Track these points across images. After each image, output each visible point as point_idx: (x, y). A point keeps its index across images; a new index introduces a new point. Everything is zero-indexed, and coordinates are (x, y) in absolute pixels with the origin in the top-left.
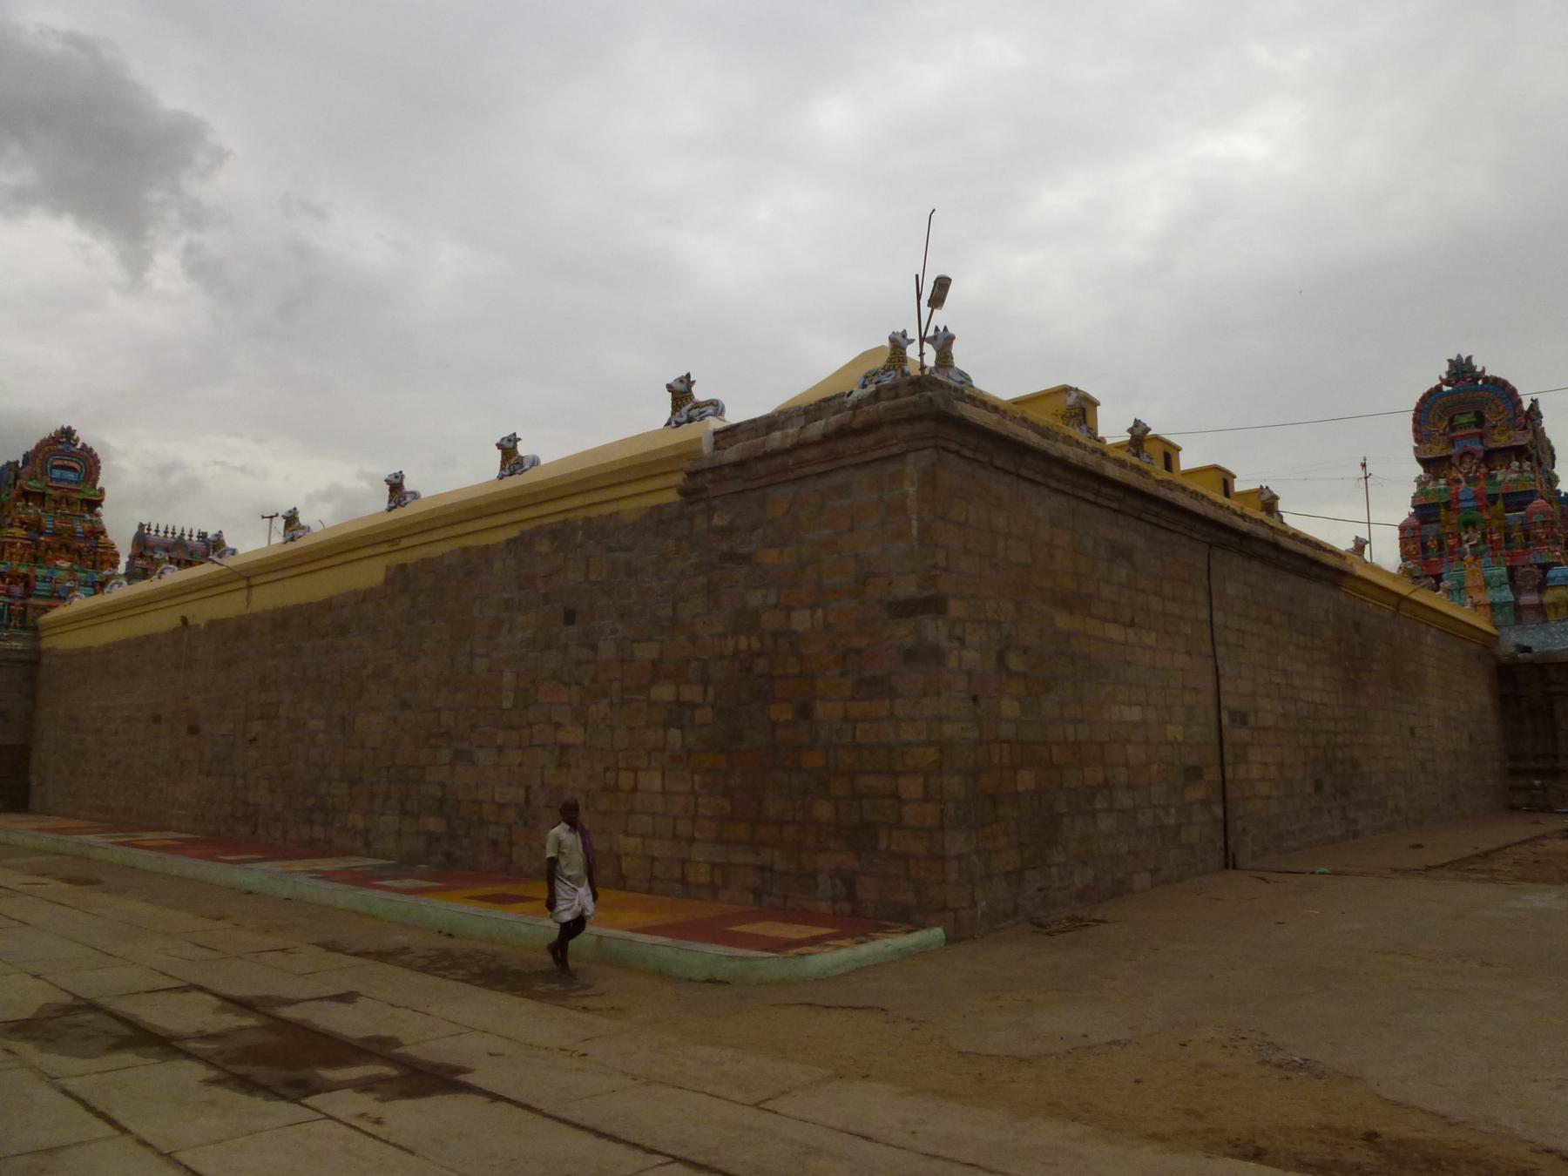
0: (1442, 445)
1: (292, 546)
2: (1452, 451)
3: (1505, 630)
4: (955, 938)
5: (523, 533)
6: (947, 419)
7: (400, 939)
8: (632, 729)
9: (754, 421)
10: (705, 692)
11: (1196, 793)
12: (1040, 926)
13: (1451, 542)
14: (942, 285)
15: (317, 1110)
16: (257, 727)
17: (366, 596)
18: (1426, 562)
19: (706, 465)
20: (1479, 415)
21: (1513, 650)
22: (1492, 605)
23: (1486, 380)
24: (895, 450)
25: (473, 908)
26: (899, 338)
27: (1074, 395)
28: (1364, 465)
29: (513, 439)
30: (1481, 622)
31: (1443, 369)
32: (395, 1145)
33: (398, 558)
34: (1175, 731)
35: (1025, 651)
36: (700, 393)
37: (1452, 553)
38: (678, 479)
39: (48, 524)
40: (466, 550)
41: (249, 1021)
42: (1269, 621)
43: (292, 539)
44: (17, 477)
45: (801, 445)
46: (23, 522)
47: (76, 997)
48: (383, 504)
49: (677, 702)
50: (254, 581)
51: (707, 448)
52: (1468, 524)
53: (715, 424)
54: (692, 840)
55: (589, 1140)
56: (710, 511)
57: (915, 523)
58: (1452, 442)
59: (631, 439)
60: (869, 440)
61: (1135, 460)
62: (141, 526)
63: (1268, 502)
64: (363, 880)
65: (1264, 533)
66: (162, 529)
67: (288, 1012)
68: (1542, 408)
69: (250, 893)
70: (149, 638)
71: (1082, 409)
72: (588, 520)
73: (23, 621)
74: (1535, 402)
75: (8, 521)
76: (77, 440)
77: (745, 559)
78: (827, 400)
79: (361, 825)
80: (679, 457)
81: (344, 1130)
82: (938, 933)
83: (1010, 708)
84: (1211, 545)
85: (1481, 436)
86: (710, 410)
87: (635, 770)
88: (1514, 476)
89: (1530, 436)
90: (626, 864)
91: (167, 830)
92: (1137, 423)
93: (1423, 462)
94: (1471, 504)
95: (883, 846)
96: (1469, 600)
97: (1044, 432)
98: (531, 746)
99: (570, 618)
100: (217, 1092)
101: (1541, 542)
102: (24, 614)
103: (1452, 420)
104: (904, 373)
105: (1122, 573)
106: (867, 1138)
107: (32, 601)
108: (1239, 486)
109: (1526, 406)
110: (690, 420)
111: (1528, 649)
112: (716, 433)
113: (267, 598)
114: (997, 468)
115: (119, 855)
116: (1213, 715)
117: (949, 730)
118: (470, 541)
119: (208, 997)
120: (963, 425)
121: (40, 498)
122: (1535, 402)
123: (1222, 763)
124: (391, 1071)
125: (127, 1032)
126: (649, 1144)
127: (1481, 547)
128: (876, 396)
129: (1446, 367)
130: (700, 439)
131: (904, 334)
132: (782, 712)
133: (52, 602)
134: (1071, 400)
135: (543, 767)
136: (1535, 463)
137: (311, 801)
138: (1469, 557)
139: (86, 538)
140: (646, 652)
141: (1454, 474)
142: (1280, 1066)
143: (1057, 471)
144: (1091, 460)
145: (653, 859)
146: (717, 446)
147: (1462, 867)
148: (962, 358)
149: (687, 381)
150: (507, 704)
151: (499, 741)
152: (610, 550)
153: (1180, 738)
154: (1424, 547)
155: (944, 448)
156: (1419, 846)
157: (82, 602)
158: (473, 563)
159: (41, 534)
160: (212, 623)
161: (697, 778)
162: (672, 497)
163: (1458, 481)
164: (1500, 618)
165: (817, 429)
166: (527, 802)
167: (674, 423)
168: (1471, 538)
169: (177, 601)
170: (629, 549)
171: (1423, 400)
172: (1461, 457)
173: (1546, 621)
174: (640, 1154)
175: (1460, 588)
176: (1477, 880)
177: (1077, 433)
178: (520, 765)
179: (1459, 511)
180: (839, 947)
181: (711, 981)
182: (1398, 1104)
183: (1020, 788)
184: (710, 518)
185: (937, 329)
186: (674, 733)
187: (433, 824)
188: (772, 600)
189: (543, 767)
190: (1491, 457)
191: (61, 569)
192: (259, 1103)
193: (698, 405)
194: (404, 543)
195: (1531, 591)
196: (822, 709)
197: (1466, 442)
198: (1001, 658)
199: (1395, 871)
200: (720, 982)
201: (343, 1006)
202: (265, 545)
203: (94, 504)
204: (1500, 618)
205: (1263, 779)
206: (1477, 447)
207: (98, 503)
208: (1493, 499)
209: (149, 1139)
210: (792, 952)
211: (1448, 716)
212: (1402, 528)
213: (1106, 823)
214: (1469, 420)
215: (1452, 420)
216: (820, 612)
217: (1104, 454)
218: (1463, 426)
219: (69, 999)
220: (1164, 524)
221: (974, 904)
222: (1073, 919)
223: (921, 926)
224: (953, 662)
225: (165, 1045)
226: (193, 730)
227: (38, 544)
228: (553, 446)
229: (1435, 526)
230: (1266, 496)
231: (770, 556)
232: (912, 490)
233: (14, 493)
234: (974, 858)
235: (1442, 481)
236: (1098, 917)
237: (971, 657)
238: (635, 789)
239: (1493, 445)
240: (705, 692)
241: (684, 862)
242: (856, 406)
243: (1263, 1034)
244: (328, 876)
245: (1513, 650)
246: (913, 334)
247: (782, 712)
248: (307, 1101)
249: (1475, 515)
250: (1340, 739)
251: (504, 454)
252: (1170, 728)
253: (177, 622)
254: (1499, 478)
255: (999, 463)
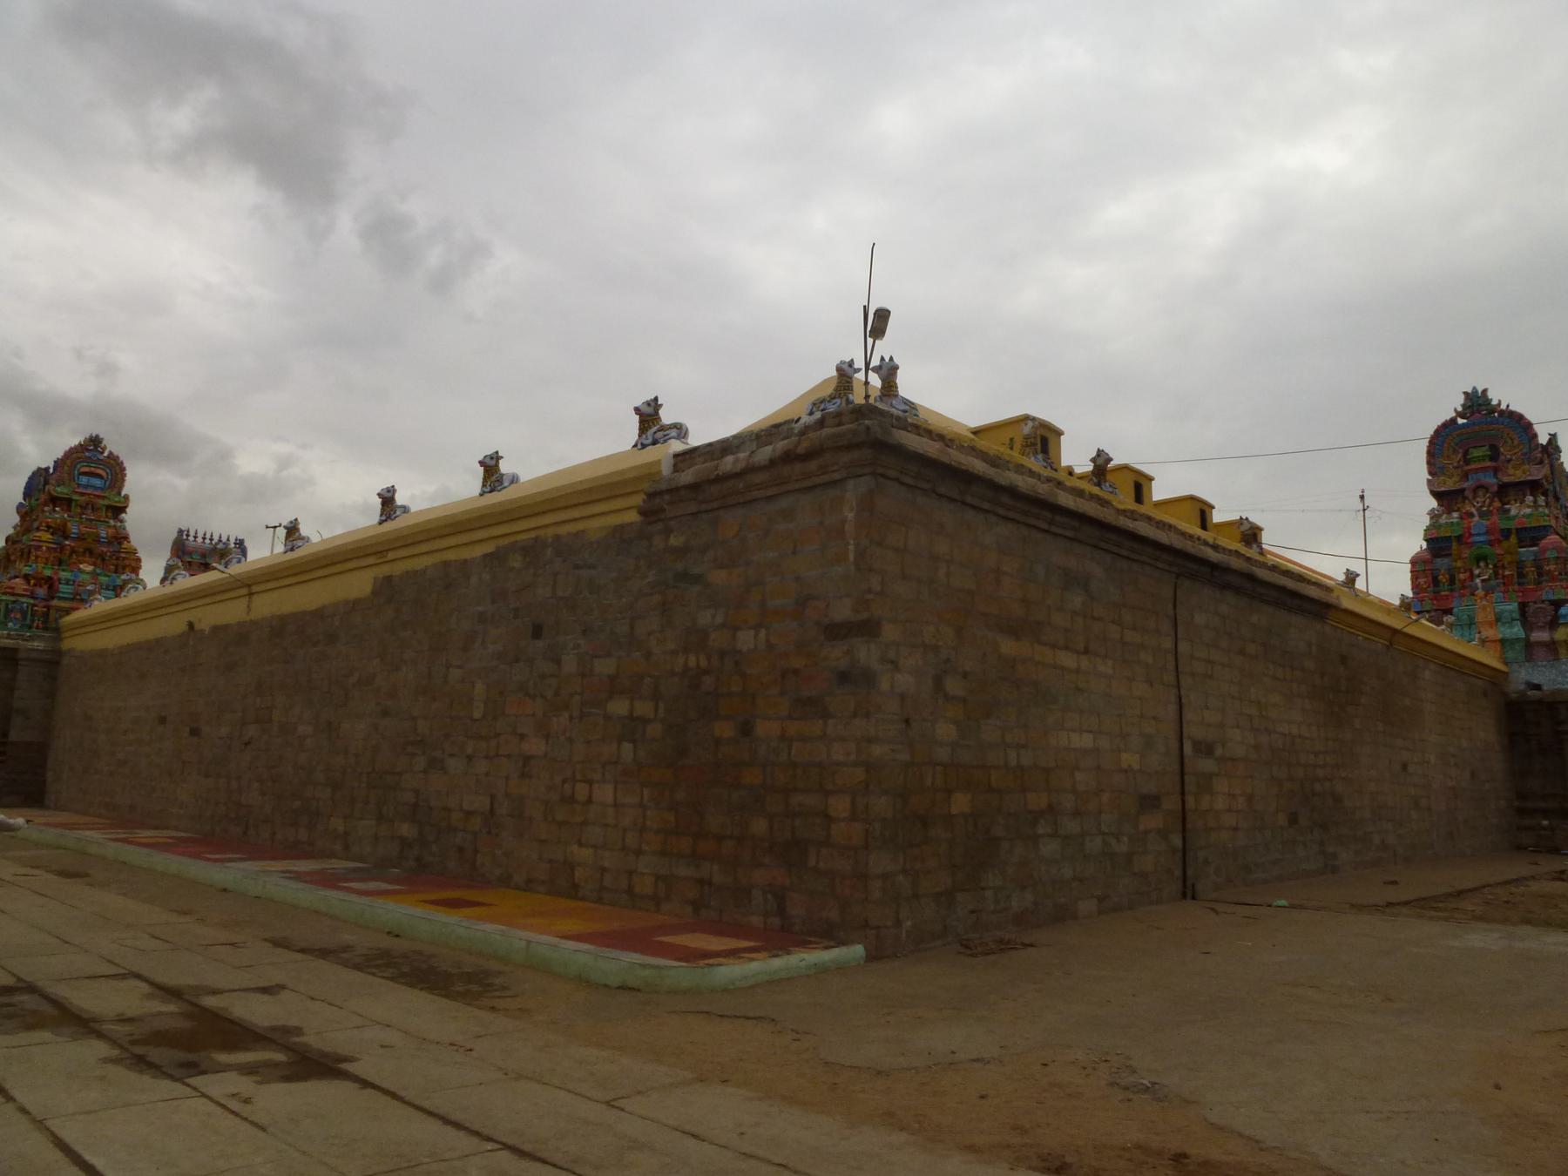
0: (1455, 479)
1: (291, 555)
2: (1466, 485)
3: (1515, 667)
4: (875, 955)
5: (498, 548)
6: (884, 447)
7: (347, 937)
8: (589, 742)
9: (710, 445)
10: (656, 710)
11: (1152, 821)
12: (967, 947)
13: (1462, 576)
14: (883, 316)
15: (195, 1089)
16: (252, 731)
17: (354, 605)
18: (1436, 596)
19: (664, 486)
20: (1494, 448)
21: (1522, 687)
22: (1503, 642)
23: (1502, 413)
24: (837, 476)
25: (419, 911)
26: (845, 367)
27: (1030, 424)
28: (1362, 497)
29: (496, 457)
30: (1490, 658)
31: (1458, 402)
32: (252, 1123)
33: (385, 570)
34: (1130, 759)
35: (965, 675)
36: (667, 417)
37: (1464, 587)
38: (638, 500)
39: (74, 529)
40: (446, 564)
41: (171, 1008)
42: (1242, 652)
43: (292, 549)
44: (46, 483)
45: (751, 469)
46: (49, 527)
47: (20, 979)
48: (375, 518)
49: (631, 717)
50: (255, 589)
51: (666, 469)
52: (1480, 558)
53: (676, 446)
54: (639, 853)
55: (435, 1126)
56: (668, 532)
57: (851, 547)
58: (1465, 476)
59: (600, 460)
60: (813, 465)
61: (1096, 490)
62: (181, 532)
63: (1251, 534)
64: (329, 881)
65: (1236, 563)
66: (200, 535)
67: (209, 1002)
68: (1561, 443)
69: (225, 890)
70: (158, 642)
71: (1043, 438)
72: (557, 537)
73: (46, 621)
74: (1553, 437)
75: (36, 525)
76: (104, 449)
77: (698, 579)
78: (777, 426)
79: (341, 829)
80: (639, 479)
81: (212, 1107)
82: (858, 950)
83: (945, 730)
84: (1178, 576)
85: (1496, 470)
86: (674, 433)
87: (590, 783)
88: (1528, 511)
89: (1546, 470)
90: (579, 874)
91: (167, 828)
92: (1100, 453)
93: (1437, 495)
94: (1482, 538)
95: (812, 862)
96: (1478, 638)
97: (994, 461)
98: (497, 755)
99: (537, 632)
100: (115, 1071)
101: (1554, 579)
102: (46, 615)
103: (1466, 453)
104: (848, 402)
105: (1077, 600)
106: (694, 1136)
107: (55, 602)
108: (1217, 517)
109: (1543, 439)
110: (655, 443)
111: (1538, 687)
112: (676, 456)
113: (267, 605)
114: (941, 496)
115: (113, 850)
116: (1174, 745)
117: (877, 750)
118: (451, 556)
119: (144, 985)
120: (898, 450)
121: (66, 503)
122: (1553, 437)
123: (1183, 794)
124: (280, 1057)
125: (46, 1008)
126: (486, 1132)
127: (1493, 582)
128: (821, 423)
129: (1461, 399)
130: (658, 462)
131: (851, 364)
132: (725, 730)
133: (74, 604)
134: (1027, 429)
135: (507, 778)
136: (1551, 499)
137: (297, 804)
138: (1480, 592)
139: (109, 543)
140: (605, 667)
141: (1468, 508)
142: (1126, 1088)
143: (1006, 499)
144: (1043, 489)
145: (604, 870)
146: (676, 468)
147: (1424, 905)
148: (907, 386)
149: (655, 404)
150: (477, 715)
151: (470, 751)
152: (577, 567)
153: (1136, 767)
154: (1436, 582)
155: (882, 475)
156: (1395, 883)
157: (101, 605)
158: (450, 576)
159: (67, 538)
160: (216, 629)
161: (646, 792)
162: (633, 517)
163: (1472, 515)
164: (1510, 655)
165: (765, 453)
166: (492, 810)
167: (640, 445)
168: (1482, 573)
169: (186, 606)
170: (592, 567)
171: (1438, 432)
172: (1475, 490)
173: (1557, 659)
174: (475, 1140)
175: (1471, 623)
176: (1431, 918)
177: (1034, 463)
178: (487, 774)
179: (1471, 545)
180: (753, 960)
181: (622, 987)
182: (1221, 1129)
183: (954, 811)
184: (668, 538)
185: (882, 359)
186: (627, 747)
187: (406, 830)
188: (719, 619)
189: (507, 778)
190: (1505, 491)
191: (83, 572)
192: (146, 1080)
193: (663, 428)
194: (391, 555)
195: (1542, 628)
196: (761, 729)
197: (1481, 476)
198: (938, 682)
199: (1353, 906)
200: (632, 989)
201: (266, 998)
202: (267, 553)
203: (118, 510)
204: (1510, 655)
205: (1230, 810)
206: (1490, 480)
207: (123, 510)
208: (1507, 534)
209: (28, 1107)
210: (702, 963)
211: (1450, 752)
212: (1414, 562)
213: (1049, 848)
214: (1479, 449)
215: (1466, 453)
216: (763, 634)
217: (1059, 484)
218: (1480, 459)
219: (11, 981)
220: (1124, 553)
221: (898, 923)
222: (1001, 941)
223: (841, 943)
224: (885, 686)
225: (82, 1024)
226: (195, 732)
227: (62, 548)
228: (537, 460)
229: (1446, 560)
230: (1245, 527)
231: (719, 577)
232: (851, 515)
233: (43, 497)
234: (901, 877)
235: (1455, 515)
236: (1027, 941)
237: (905, 681)
238: (590, 801)
239: (1506, 479)
240: (656, 710)
241: (630, 873)
242: (807, 429)
243: (1129, 1058)
244: (299, 877)
245: (1522, 687)
246: (860, 363)
247: (725, 730)
248: (190, 1081)
249: (1487, 549)
250: (1320, 772)
251: (486, 471)
252: (1124, 756)
253: (183, 627)
254: (1513, 512)
255: (942, 490)
